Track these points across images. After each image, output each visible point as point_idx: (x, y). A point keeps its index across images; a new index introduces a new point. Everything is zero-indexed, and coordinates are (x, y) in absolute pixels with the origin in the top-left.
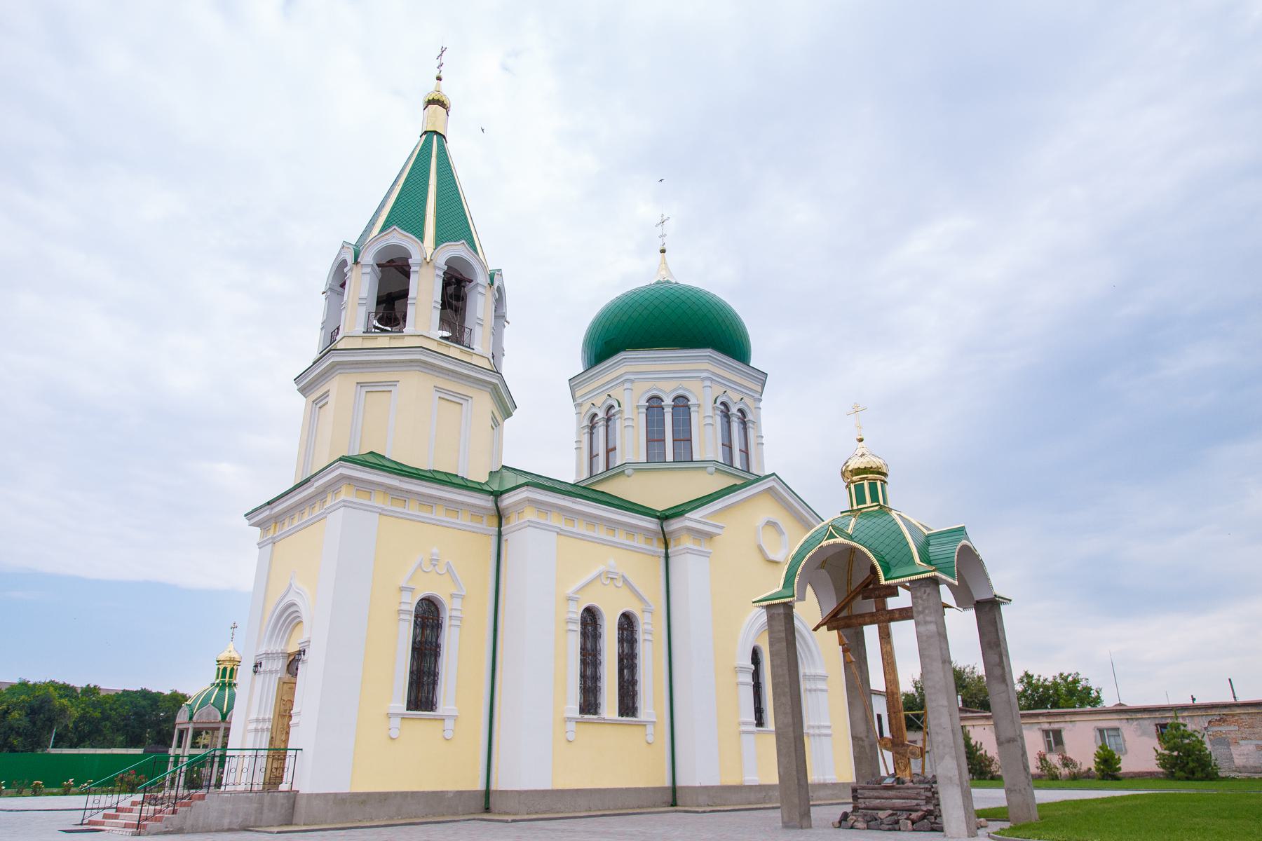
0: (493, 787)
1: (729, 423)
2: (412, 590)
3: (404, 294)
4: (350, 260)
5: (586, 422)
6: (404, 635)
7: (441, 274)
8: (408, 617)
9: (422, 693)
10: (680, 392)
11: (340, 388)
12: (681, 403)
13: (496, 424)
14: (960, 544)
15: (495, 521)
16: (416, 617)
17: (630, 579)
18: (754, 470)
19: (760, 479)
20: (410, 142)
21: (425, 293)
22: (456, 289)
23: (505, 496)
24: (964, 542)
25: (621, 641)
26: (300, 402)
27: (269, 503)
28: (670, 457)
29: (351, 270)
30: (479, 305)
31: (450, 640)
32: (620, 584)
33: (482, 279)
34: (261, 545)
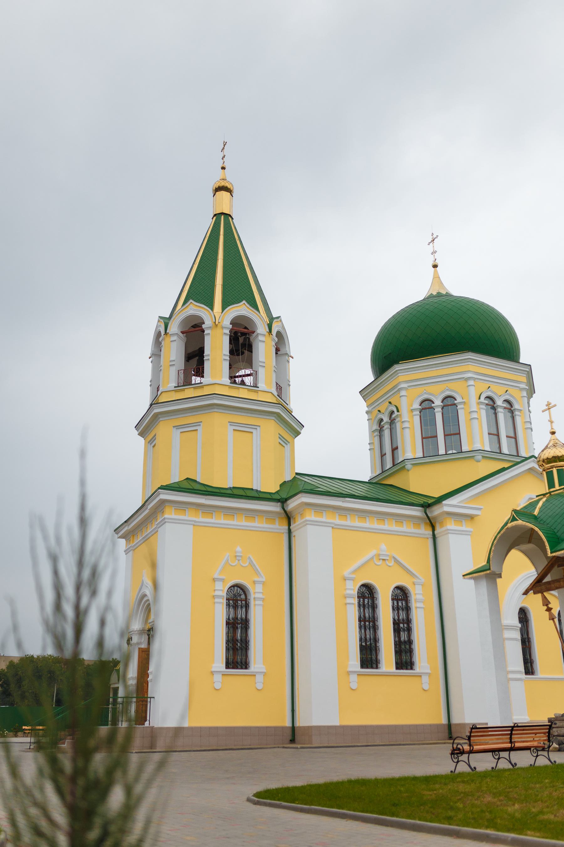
0: (297, 724)
1: (496, 414)
2: (222, 580)
5: (376, 427)
6: (220, 614)
7: (228, 332)
8: (221, 600)
9: (237, 654)
10: (448, 393)
11: (165, 430)
12: (449, 402)
13: (284, 442)
15: (285, 522)
16: (228, 599)
19: (527, 459)
20: (208, 222)
21: (217, 348)
22: (241, 343)
25: (396, 609)
26: (141, 440)
27: (126, 522)
28: (442, 451)
29: (163, 339)
30: (263, 349)
31: (257, 616)
32: (392, 563)
33: (261, 329)
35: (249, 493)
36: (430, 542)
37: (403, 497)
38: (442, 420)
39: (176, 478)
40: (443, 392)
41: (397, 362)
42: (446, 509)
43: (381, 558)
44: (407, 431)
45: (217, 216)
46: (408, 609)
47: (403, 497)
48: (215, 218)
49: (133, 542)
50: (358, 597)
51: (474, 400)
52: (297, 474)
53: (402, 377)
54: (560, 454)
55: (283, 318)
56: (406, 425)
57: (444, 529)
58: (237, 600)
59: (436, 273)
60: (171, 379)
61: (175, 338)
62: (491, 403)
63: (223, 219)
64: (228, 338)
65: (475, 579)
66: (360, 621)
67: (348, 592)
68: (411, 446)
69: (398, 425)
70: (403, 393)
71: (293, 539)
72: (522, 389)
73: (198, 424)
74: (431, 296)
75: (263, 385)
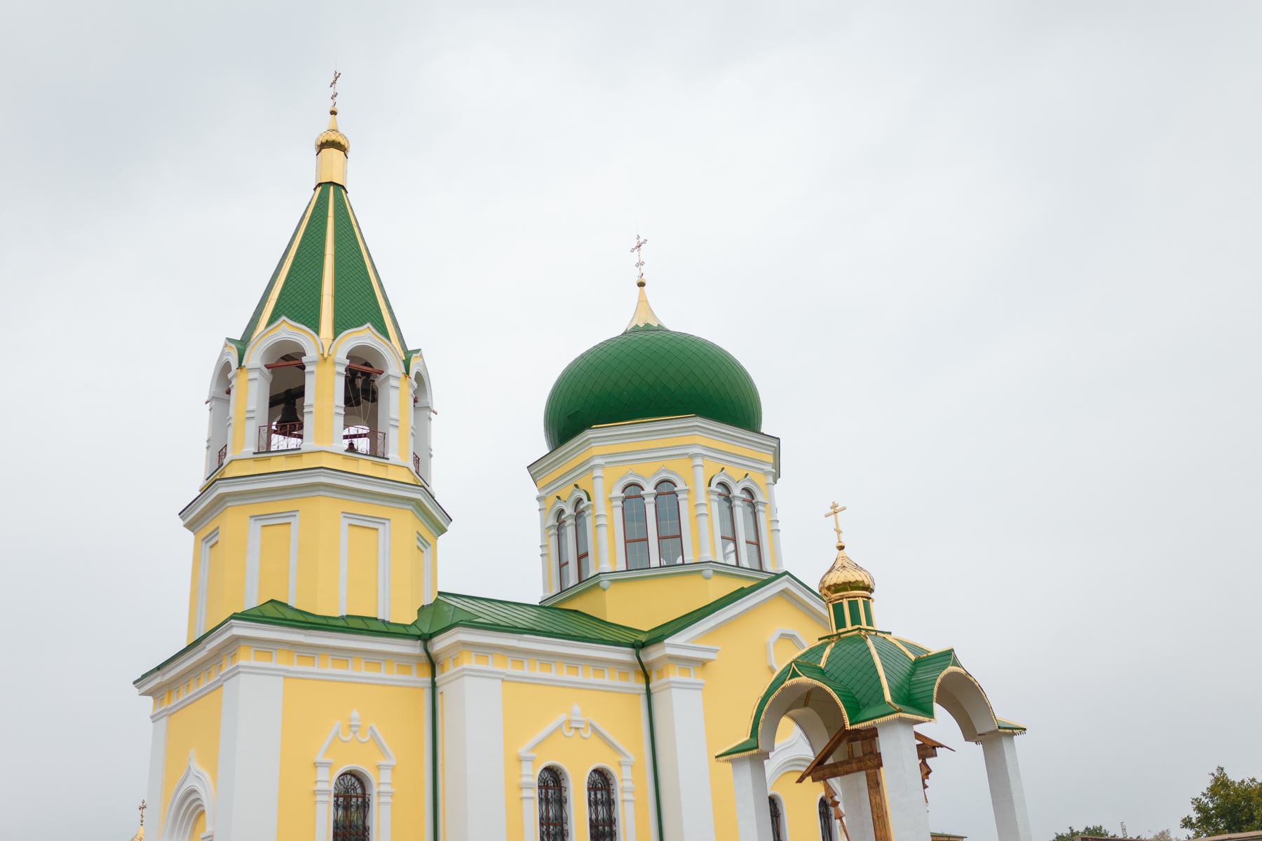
1: (731, 508)
2: (329, 765)
3: (300, 392)
4: (234, 365)
5: (552, 521)
7: (342, 370)
8: (326, 798)
10: (664, 476)
11: (236, 523)
12: (666, 489)
14: (945, 672)
15: (428, 670)
16: (337, 796)
17: (600, 727)
18: (769, 567)
19: (778, 576)
20: (305, 196)
22: (362, 388)
23: (435, 640)
24: (951, 669)
25: (593, 803)
26: (190, 535)
27: (158, 668)
28: (655, 562)
30: (394, 399)
32: (588, 733)
33: (394, 367)
34: (155, 718)
35: (374, 626)
36: (643, 700)
37: (595, 630)
38: (653, 517)
39: (252, 601)
40: (657, 474)
41: (589, 427)
42: (669, 651)
43: (574, 725)
44: (603, 531)
45: (323, 186)
46: (610, 803)
47: (595, 630)
48: (319, 189)
49: (169, 702)
50: (540, 787)
51: (702, 486)
52: (440, 593)
53: (597, 449)
54: (852, 580)
55: (424, 352)
56: (602, 521)
57: (664, 680)
58: (351, 797)
59: (642, 295)
60: (244, 441)
61: (255, 375)
62: (725, 492)
63: (330, 193)
64: (343, 379)
65: (731, 761)
66: (541, 824)
67: (525, 780)
68: (608, 553)
69: (589, 521)
70: (597, 472)
71: (439, 697)
72: (766, 473)
73: (292, 514)
74: (636, 329)
75: (396, 456)
